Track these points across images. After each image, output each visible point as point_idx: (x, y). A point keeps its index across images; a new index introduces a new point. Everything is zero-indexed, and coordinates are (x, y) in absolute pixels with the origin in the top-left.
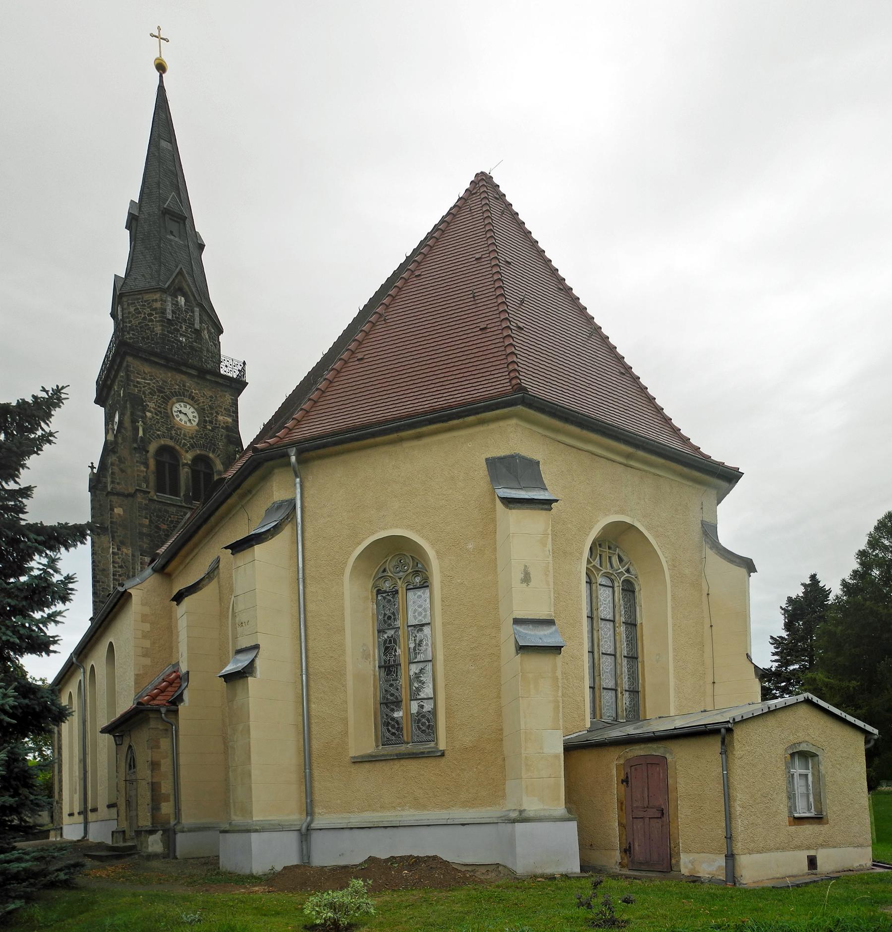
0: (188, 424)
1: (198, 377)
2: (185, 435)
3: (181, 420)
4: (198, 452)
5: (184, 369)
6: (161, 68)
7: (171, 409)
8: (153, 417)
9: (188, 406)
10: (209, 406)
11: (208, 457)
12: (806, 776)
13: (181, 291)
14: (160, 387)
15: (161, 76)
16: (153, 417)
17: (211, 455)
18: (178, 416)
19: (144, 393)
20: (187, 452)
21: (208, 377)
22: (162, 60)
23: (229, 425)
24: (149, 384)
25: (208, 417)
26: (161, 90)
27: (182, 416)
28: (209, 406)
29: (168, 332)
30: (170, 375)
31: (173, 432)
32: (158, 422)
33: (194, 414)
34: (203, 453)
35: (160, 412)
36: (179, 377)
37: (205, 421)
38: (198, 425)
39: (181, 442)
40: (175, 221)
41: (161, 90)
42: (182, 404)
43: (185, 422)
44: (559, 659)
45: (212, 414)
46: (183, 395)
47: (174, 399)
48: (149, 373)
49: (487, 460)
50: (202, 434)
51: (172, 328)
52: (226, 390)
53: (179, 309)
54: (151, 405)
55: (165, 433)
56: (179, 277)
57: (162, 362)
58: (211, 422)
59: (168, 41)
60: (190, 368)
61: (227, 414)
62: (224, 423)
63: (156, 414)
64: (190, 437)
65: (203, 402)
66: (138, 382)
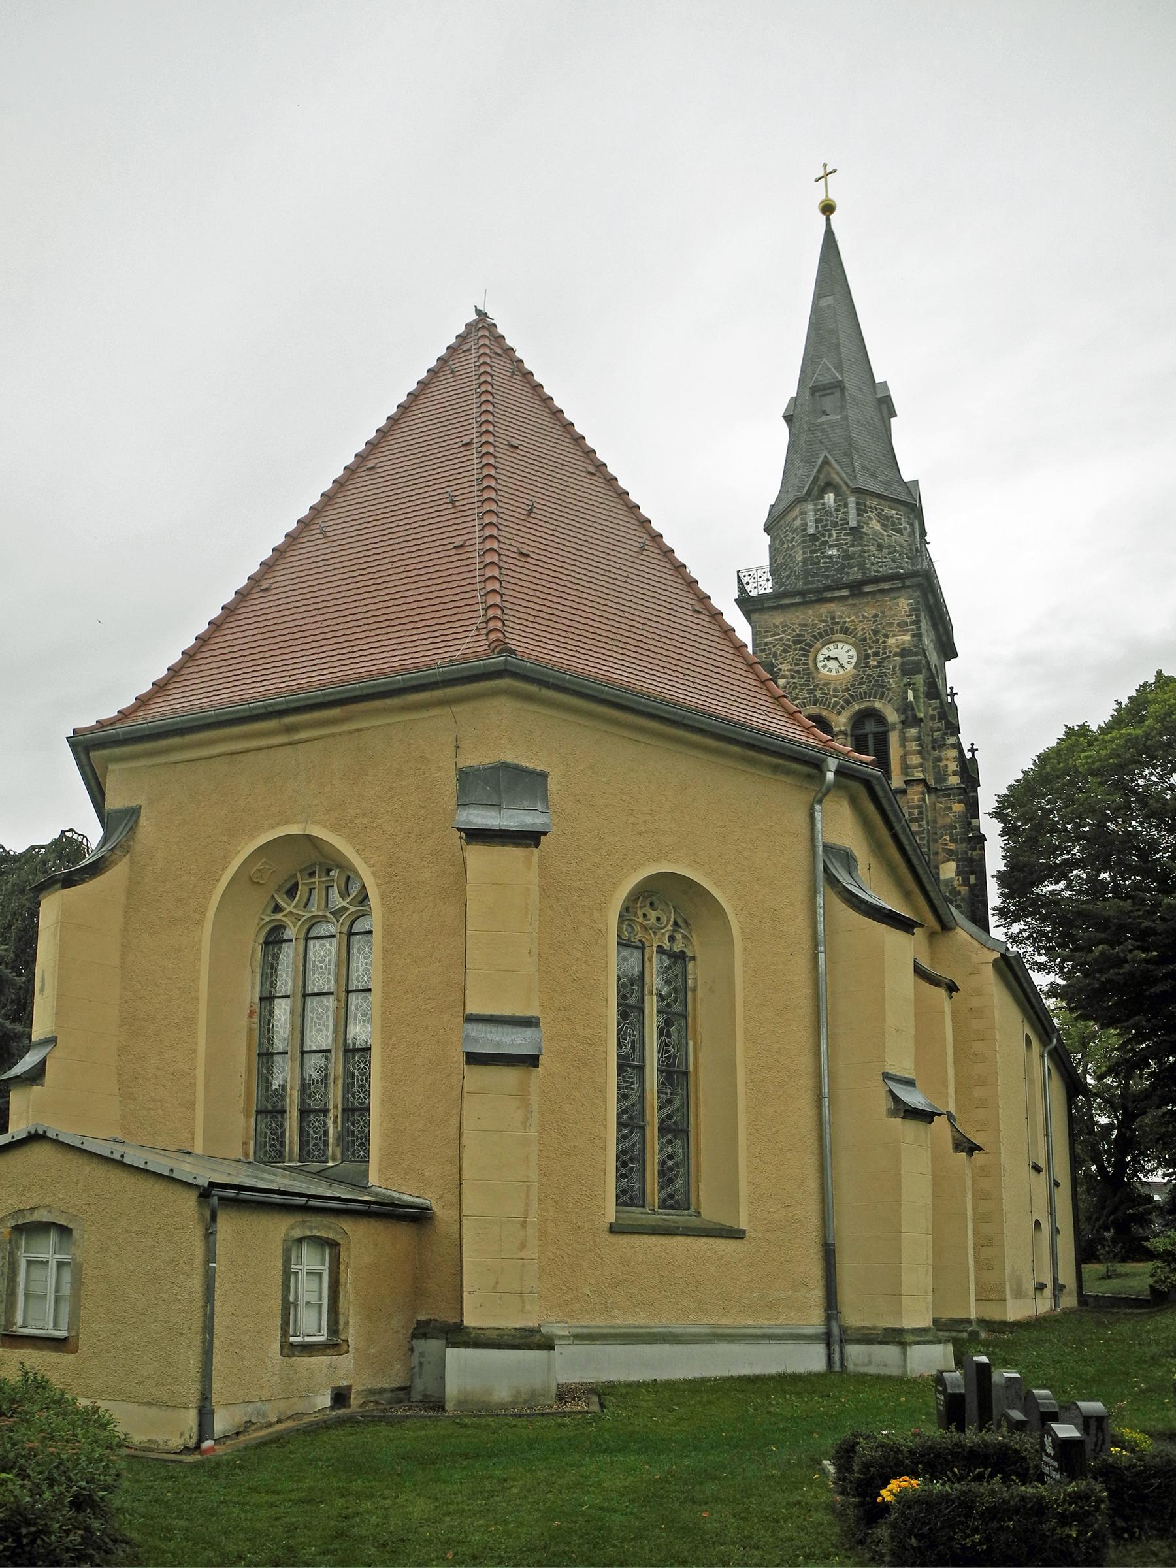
0: (841, 671)
1: (852, 595)
2: (835, 690)
3: (830, 670)
4: (857, 707)
5: (829, 595)
6: (828, 209)
7: (815, 660)
8: (788, 683)
9: (840, 645)
10: (872, 630)
11: (875, 710)
12: (320, 1275)
13: (829, 486)
14: (798, 635)
15: (828, 220)
16: (788, 683)
17: (878, 705)
18: (824, 667)
19: (775, 655)
20: (839, 713)
21: (867, 589)
22: (830, 200)
23: (907, 645)
24: (781, 639)
25: (871, 648)
26: (829, 235)
27: (833, 664)
28: (872, 630)
29: (811, 552)
30: (810, 612)
31: (818, 693)
32: (795, 688)
33: (850, 653)
34: (865, 705)
35: (798, 672)
36: (823, 609)
37: (868, 656)
38: (854, 668)
39: (830, 703)
40: (828, 394)
41: (829, 235)
42: (831, 646)
43: (837, 671)
44: (537, 1077)
45: (877, 641)
46: (826, 636)
47: (818, 645)
48: (782, 623)
49: (956, 655)
50: (862, 678)
51: (817, 543)
52: (898, 595)
53: (827, 513)
54: (785, 667)
55: (806, 698)
56: (826, 468)
57: (797, 600)
58: (876, 654)
59: (835, 171)
60: (835, 589)
61: (903, 631)
62: (897, 647)
63: (793, 677)
64: (843, 691)
65: (863, 629)
66: (766, 644)
